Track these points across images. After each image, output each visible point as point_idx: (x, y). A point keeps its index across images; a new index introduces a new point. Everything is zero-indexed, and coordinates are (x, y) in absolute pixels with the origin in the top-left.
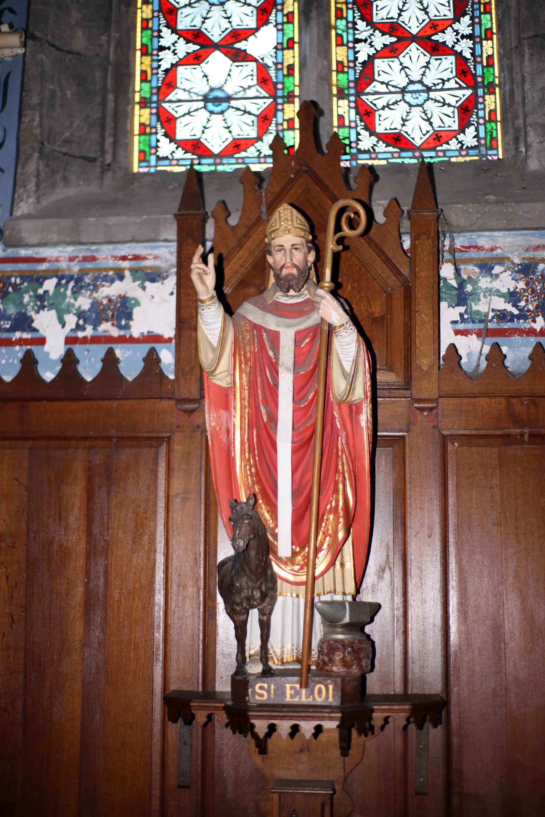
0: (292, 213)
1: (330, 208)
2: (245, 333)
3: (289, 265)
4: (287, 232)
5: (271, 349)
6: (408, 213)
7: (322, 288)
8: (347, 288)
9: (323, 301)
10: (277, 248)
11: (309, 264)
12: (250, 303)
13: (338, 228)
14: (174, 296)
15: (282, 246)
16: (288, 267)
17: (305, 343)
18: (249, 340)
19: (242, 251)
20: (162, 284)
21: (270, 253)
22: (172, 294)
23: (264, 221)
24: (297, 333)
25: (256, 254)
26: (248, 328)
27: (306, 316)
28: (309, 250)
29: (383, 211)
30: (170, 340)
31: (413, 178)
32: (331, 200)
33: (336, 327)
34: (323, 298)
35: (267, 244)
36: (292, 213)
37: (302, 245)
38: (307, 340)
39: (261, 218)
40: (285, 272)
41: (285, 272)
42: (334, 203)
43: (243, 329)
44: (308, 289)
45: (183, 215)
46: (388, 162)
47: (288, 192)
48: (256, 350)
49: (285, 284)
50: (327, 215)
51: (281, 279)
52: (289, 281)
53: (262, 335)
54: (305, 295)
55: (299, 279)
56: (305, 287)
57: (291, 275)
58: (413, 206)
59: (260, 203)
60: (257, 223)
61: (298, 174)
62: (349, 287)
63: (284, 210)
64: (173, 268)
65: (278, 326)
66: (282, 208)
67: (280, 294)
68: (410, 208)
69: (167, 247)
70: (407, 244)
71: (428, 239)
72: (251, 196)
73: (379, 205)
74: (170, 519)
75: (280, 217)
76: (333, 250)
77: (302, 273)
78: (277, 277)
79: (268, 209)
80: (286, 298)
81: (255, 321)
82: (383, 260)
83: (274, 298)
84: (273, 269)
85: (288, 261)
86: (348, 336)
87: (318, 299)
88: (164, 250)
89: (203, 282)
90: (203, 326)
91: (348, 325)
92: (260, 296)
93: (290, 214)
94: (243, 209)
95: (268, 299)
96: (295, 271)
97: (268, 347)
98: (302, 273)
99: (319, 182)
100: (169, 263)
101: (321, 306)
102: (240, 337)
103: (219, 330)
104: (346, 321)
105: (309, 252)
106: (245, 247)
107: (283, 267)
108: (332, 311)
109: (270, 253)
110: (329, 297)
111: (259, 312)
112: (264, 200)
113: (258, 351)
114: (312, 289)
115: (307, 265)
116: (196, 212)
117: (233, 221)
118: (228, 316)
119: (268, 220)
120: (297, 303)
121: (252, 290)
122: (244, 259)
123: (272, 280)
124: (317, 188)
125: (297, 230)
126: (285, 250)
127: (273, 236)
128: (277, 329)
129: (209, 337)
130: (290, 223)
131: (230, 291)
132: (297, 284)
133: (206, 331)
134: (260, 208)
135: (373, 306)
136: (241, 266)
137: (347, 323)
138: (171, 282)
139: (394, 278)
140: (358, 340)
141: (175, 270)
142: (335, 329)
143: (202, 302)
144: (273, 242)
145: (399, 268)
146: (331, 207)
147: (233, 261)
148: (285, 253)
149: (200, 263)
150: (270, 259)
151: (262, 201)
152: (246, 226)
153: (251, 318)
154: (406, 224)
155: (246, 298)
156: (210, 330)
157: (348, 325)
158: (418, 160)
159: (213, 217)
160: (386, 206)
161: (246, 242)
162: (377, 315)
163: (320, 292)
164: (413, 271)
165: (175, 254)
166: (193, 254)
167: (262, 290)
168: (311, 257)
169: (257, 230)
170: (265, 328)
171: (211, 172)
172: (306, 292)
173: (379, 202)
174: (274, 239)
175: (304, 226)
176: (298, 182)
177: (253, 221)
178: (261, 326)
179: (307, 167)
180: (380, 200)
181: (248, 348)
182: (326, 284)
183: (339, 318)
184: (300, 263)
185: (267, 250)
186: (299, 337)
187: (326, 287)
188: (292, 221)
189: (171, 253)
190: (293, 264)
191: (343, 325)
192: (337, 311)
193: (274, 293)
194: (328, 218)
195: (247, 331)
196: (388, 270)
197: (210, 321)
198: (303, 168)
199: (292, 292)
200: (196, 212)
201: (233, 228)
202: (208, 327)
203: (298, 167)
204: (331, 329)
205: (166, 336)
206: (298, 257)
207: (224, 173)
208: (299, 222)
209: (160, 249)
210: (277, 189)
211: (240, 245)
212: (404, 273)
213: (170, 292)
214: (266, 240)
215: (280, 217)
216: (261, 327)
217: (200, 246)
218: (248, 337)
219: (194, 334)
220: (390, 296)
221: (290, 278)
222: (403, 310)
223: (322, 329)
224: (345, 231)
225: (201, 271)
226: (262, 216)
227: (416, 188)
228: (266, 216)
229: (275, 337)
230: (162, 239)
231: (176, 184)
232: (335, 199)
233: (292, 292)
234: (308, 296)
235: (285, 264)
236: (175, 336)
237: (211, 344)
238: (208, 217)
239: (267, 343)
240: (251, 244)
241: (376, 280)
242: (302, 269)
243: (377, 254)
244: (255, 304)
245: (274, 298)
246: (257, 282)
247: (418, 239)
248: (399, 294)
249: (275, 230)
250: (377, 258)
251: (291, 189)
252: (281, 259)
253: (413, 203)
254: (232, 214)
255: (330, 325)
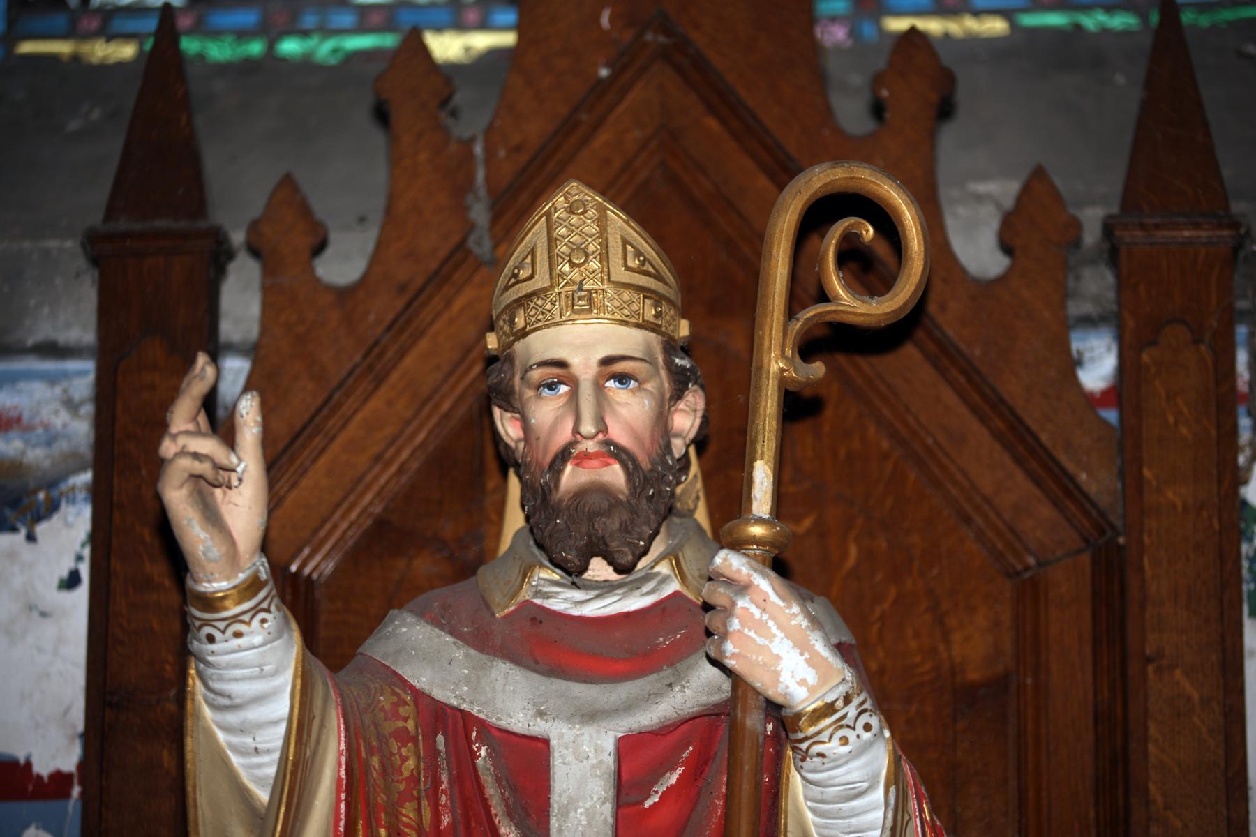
0: (602, 222)
1: (768, 208)
2: (395, 746)
3: (590, 446)
4: (581, 304)
5: (510, 814)
6: (1108, 228)
7: (737, 545)
8: (845, 555)
9: (742, 603)
10: (536, 374)
11: (678, 446)
12: (423, 615)
13: (807, 289)
14: (81, 595)
15: (562, 364)
16: (586, 456)
17: (661, 788)
18: (414, 779)
19: (384, 392)
20: (31, 538)
21: (509, 400)
22: (72, 581)
23: (479, 264)
24: (627, 747)
25: (446, 406)
26: (410, 725)
27: (667, 672)
28: (681, 381)
29: (995, 224)
30: (60, 782)
31: (1126, 89)
32: (771, 176)
33: (798, 716)
34: (743, 588)
35: (491, 360)
36: (602, 222)
37: (648, 359)
38: (673, 778)
39: (468, 253)
40: (571, 477)
41: (571, 477)
42: (781, 187)
43: (389, 727)
44: (672, 554)
45: (126, 235)
46: (1013, 25)
47: (585, 141)
48: (446, 820)
49: (572, 536)
50: (758, 241)
51: (556, 510)
52: (592, 517)
53: (473, 756)
54: (660, 582)
55: (634, 512)
56: (658, 547)
57: (602, 489)
58: (1129, 202)
59: (461, 189)
60: (451, 285)
61: (627, 63)
62: (853, 551)
63: (571, 210)
64: (83, 469)
65: (541, 714)
66: (560, 200)
67: (547, 574)
68: (1115, 210)
69: (52, 379)
70: (1098, 367)
71: (1197, 341)
72: (423, 157)
73: (979, 199)
74: (313, 409)
75: (551, 241)
76: (782, 380)
77: (647, 482)
78: (539, 501)
79: (496, 216)
80: (578, 595)
81: (439, 695)
82: (997, 436)
83: (526, 594)
84: (517, 466)
85: (588, 428)
86: (853, 756)
87: (719, 595)
88: (39, 390)
89: (213, 517)
90: (207, 712)
91: (852, 710)
92: (459, 586)
93: (593, 229)
94: (389, 210)
95: (497, 597)
96: (615, 475)
97: (497, 809)
98: (647, 482)
99: (720, 100)
100: (63, 446)
101: (735, 624)
102: (375, 761)
103: (282, 728)
104: (842, 689)
105: (678, 395)
106: (395, 376)
107: (564, 455)
108: (785, 648)
109: (509, 400)
110: (765, 584)
111: (460, 653)
112: (480, 175)
113: (452, 825)
114: (690, 556)
115: (668, 448)
116: (182, 224)
117: (342, 266)
118: (319, 668)
119: (498, 263)
120: (627, 615)
121: (424, 565)
122: (389, 431)
123: (515, 520)
124: (712, 123)
125: (626, 295)
126: (574, 383)
127: (520, 321)
128: (539, 728)
129: (235, 760)
130: (594, 265)
131: (329, 567)
132: (625, 529)
133: (221, 736)
134: (463, 210)
135: (956, 637)
136: (378, 458)
137: (847, 700)
138: (69, 533)
139: (1046, 511)
140: (895, 778)
141: (86, 477)
142: (797, 729)
143: (210, 603)
144: (519, 346)
145: (1070, 466)
146: (772, 204)
147: (343, 438)
148: (574, 395)
149: (198, 433)
150: (509, 428)
151: (471, 179)
152: (402, 288)
153: (422, 678)
154: (1096, 284)
155: (400, 596)
156: (241, 730)
157: (852, 710)
158: (1144, 18)
159: (254, 251)
160: (1009, 203)
161: (402, 353)
162: (973, 675)
163: (730, 562)
164: (1132, 484)
165: (88, 409)
166: (172, 395)
167: (467, 558)
168: (686, 420)
169: (448, 303)
170: (483, 725)
171: (247, 67)
172: (664, 568)
173: (982, 188)
174: (524, 334)
175: (658, 277)
176: (630, 98)
177: (434, 265)
178: (466, 715)
179: (667, 32)
180: (983, 177)
181: (408, 811)
182: (757, 530)
183: (811, 677)
184: (637, 438)
185: (495, 383)
186: (635, 761)
187: (755, 540)
188: (604, 257)
189: (71, 405)
190: (608, 443)
191: (829, 709)
192: (802, 646)
193: (526, 573)
194: (758, 254)
195: (403, 737)
196: (1020, 476)
197: (240, 689)
198: (649, 37)
199: (599, 569)
200: (182, 224)
201: (344, 294)
202: (232, 718)
203: (628, 36)
204: (784, 722)
205: (43, 768)
206: (630, 411)
207: (306, 65)
208: (633, 263)
209: (22, 385)
210: (535, 129)
211: (374, 367)
212: (1093, 490)
213: (65, 573)
214: (492, 341)
215: (551, 241)
216: (467, 719)
217: (202, 359)
218: (411, 763)
219: (167, 759)
220: (1030, 592)
221: (595, 501)
222: (1088, 650)
223: (735, 729)
224: (838, 297)
225: (204, 468)
226: (471, 243)
227: (1141, 125)
228: (487, 244)
229: (529, 761)
230: (30, 342)
231: (96, 114)
232: (784, 171)
233: (599, 569)
234: (674, 586)
235: (573, 444)
236: (82, 766)
237: (243, 794)
238: (230, 256)
239: (491, 791)
240: (419, 363)
241: (968, 520)
242: (645, 465)
243: (974, 409)
244: (443, 620)
245: (526, 594)
246: (448, 529)
247: (1153, 343)
248: (1070, 583)
249: (531, 296)
250: (975, 426)
251: (596, 126)
252: (557, 422)
253: (1128, 189)
254: (335, 238)
255: (774, 709)
